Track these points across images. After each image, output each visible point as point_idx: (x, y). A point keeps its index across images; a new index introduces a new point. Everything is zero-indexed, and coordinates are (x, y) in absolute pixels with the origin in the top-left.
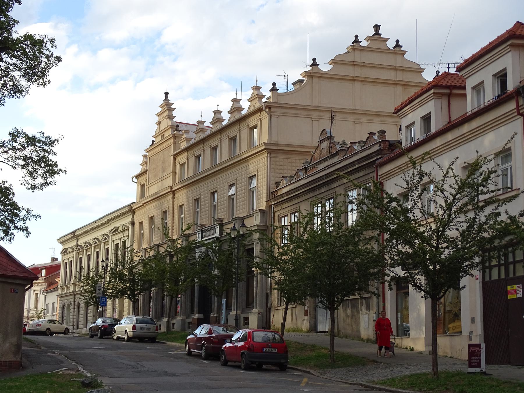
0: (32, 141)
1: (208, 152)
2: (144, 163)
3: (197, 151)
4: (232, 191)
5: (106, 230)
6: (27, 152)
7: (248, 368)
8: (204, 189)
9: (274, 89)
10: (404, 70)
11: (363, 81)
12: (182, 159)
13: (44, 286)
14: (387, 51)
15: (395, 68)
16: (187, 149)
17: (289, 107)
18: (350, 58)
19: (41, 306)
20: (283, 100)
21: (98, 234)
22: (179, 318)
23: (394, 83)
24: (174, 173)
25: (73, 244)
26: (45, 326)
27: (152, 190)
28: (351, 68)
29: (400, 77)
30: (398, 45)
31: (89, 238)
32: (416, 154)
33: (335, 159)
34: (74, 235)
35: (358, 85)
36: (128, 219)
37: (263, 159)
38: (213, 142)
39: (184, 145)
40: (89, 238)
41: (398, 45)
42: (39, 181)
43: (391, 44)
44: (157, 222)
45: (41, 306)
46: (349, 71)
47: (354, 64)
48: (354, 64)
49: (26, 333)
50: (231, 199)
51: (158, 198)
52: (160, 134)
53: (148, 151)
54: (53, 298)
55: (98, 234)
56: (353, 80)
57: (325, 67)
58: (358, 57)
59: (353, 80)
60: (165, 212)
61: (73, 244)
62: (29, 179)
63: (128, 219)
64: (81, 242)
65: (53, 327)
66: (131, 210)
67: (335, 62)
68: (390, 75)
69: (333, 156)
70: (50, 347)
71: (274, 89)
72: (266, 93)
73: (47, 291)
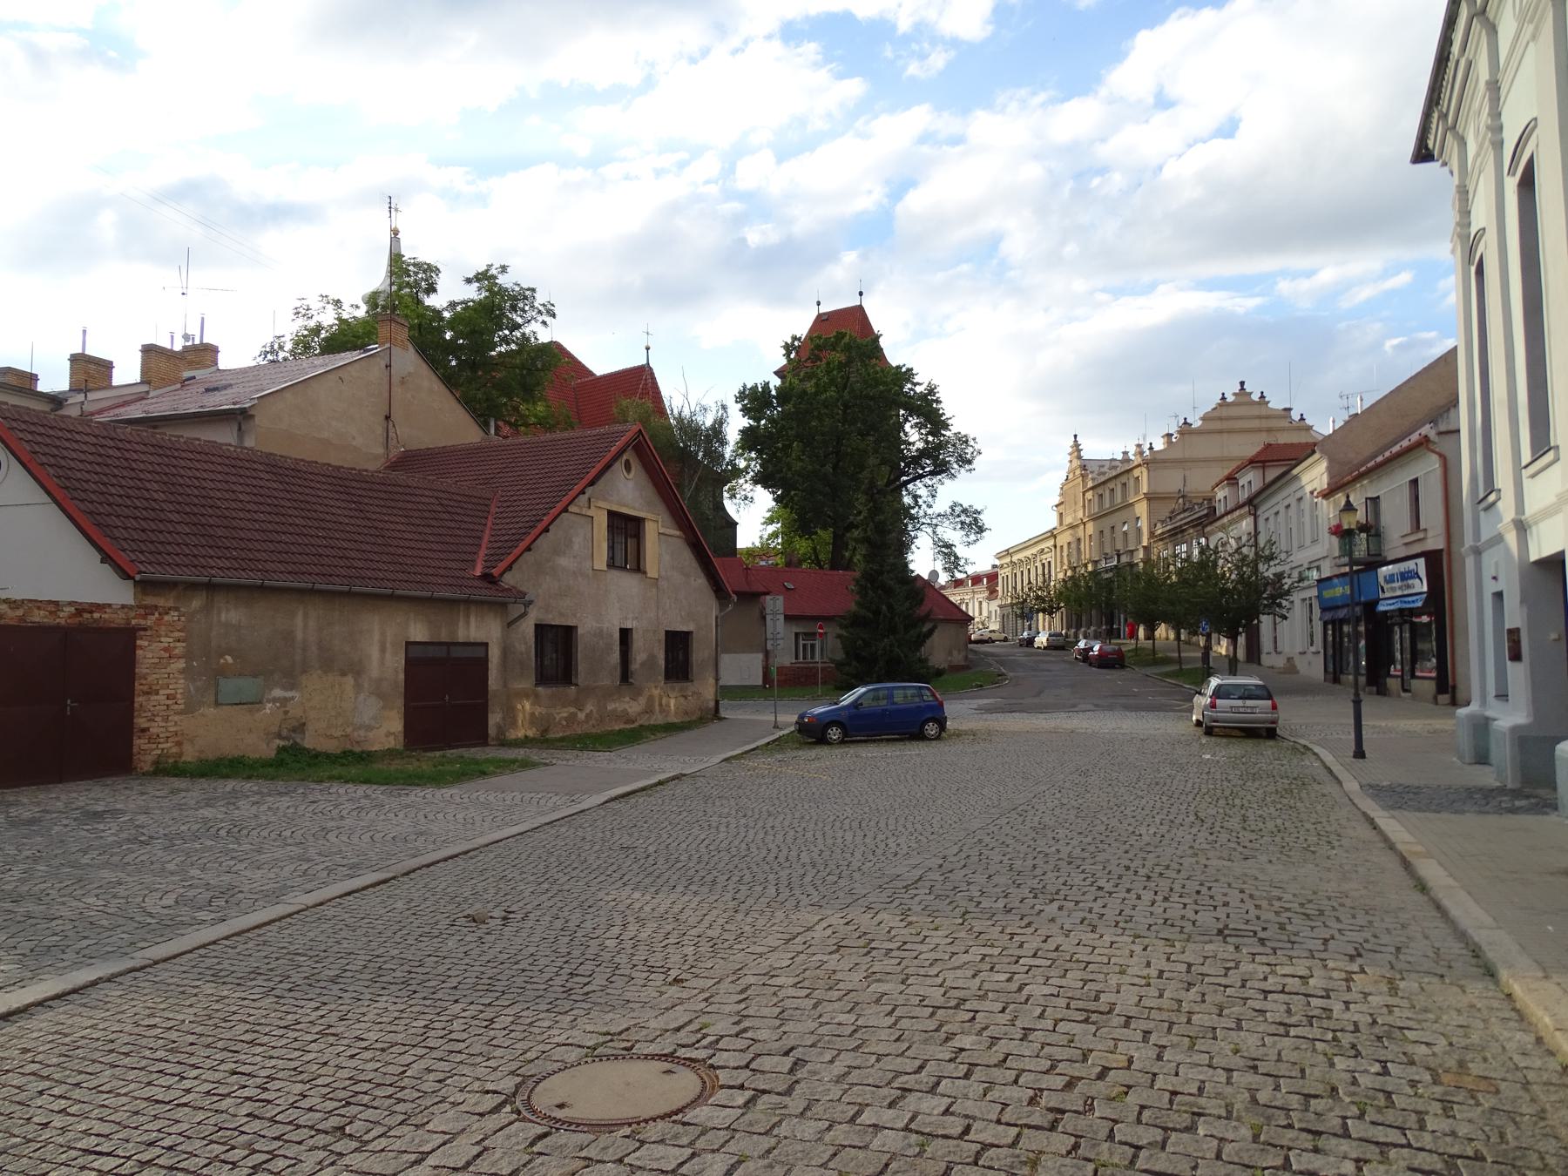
0: (965, 511)
1: (1107, 492)
2: (1061, 495)
3: (1100, 491)
4: (1125, 528)
5: (1034, 550)
6: (963, 518)
7: (1100, 667)
8: (1106, 523)
9: (1151, 448)
10: (1268, 417)
11: (1230, 432)
12: (1089, 495)
13: (986, 594)
14: (1254, 403)
15: (1259, 417)
16: (1092, 488)
17: (1164, 461)
18: (1216, 414)
19: (985, 613)
20: (1158, 457)
21: (1028, 553)
22: (1092, 628)
23: (1260, 430)
24: (1084, 506)
25: (1007, 560)
26: (987, 636)
27: (1068, 520)
28: (1219, 423)
29: (1265, 424)
30: (1262, 397)
31: (1021, 556)
32: (1225, 520)
33: (1186, 514)
34: (1008, 552)
35: (1225, 435)
36: (1050, 543)
37: (1144, 505)
38: (1111, 485)
39: (1090, 484)
40: (1021, 556)
41: (1262, 397)
42: (973, 537)
43: (1255, 397)
44: (1074, 546)
45: (985, 613)
46: (1218, 425)
47: (1220, 419)
48: (1220, 419)
49: (971, 642)
50: (1125, 533)
51: (1072, 527)
52: (1072, 471)
53: (1063, 485)
54: (994, 605)
55: (1028, 553)
56: (1221, 432)
57: (1197, 424)
58: (1225, 412)
59: (1221, 432)
60: (1079, 540)
61: (1007, 560)
62: (965, 539)
63: (1050, 543)
64: (1015, 559)
65: (994, 636)
66: (1052, 534)
67: (1202, 419)
68: (1256, 424)
69: (1185, 511)
70: (987, 654)
71: (1151, 448)
72: (1146, 448)
73: (989, 599)
